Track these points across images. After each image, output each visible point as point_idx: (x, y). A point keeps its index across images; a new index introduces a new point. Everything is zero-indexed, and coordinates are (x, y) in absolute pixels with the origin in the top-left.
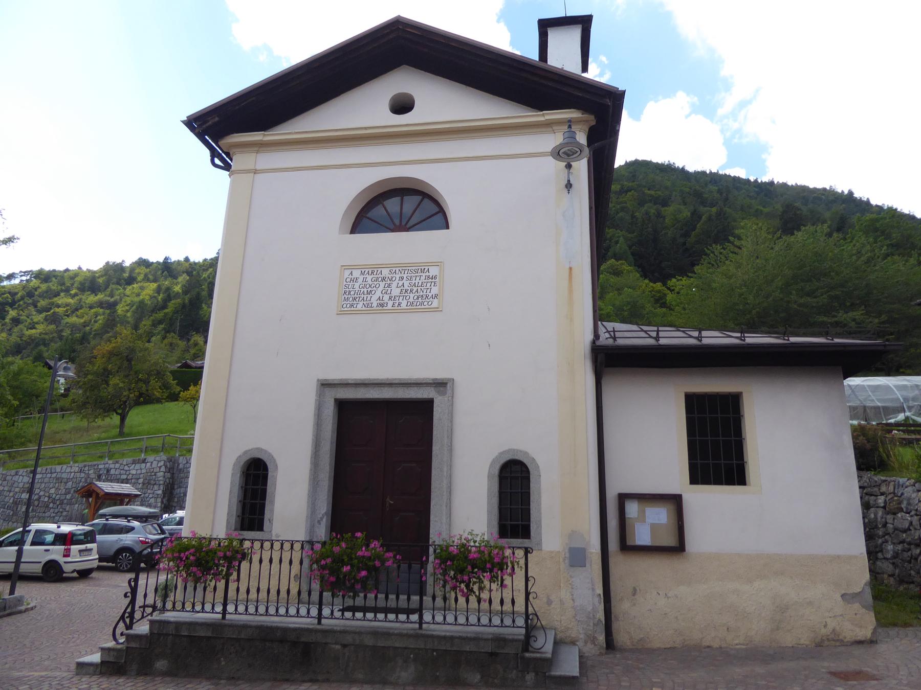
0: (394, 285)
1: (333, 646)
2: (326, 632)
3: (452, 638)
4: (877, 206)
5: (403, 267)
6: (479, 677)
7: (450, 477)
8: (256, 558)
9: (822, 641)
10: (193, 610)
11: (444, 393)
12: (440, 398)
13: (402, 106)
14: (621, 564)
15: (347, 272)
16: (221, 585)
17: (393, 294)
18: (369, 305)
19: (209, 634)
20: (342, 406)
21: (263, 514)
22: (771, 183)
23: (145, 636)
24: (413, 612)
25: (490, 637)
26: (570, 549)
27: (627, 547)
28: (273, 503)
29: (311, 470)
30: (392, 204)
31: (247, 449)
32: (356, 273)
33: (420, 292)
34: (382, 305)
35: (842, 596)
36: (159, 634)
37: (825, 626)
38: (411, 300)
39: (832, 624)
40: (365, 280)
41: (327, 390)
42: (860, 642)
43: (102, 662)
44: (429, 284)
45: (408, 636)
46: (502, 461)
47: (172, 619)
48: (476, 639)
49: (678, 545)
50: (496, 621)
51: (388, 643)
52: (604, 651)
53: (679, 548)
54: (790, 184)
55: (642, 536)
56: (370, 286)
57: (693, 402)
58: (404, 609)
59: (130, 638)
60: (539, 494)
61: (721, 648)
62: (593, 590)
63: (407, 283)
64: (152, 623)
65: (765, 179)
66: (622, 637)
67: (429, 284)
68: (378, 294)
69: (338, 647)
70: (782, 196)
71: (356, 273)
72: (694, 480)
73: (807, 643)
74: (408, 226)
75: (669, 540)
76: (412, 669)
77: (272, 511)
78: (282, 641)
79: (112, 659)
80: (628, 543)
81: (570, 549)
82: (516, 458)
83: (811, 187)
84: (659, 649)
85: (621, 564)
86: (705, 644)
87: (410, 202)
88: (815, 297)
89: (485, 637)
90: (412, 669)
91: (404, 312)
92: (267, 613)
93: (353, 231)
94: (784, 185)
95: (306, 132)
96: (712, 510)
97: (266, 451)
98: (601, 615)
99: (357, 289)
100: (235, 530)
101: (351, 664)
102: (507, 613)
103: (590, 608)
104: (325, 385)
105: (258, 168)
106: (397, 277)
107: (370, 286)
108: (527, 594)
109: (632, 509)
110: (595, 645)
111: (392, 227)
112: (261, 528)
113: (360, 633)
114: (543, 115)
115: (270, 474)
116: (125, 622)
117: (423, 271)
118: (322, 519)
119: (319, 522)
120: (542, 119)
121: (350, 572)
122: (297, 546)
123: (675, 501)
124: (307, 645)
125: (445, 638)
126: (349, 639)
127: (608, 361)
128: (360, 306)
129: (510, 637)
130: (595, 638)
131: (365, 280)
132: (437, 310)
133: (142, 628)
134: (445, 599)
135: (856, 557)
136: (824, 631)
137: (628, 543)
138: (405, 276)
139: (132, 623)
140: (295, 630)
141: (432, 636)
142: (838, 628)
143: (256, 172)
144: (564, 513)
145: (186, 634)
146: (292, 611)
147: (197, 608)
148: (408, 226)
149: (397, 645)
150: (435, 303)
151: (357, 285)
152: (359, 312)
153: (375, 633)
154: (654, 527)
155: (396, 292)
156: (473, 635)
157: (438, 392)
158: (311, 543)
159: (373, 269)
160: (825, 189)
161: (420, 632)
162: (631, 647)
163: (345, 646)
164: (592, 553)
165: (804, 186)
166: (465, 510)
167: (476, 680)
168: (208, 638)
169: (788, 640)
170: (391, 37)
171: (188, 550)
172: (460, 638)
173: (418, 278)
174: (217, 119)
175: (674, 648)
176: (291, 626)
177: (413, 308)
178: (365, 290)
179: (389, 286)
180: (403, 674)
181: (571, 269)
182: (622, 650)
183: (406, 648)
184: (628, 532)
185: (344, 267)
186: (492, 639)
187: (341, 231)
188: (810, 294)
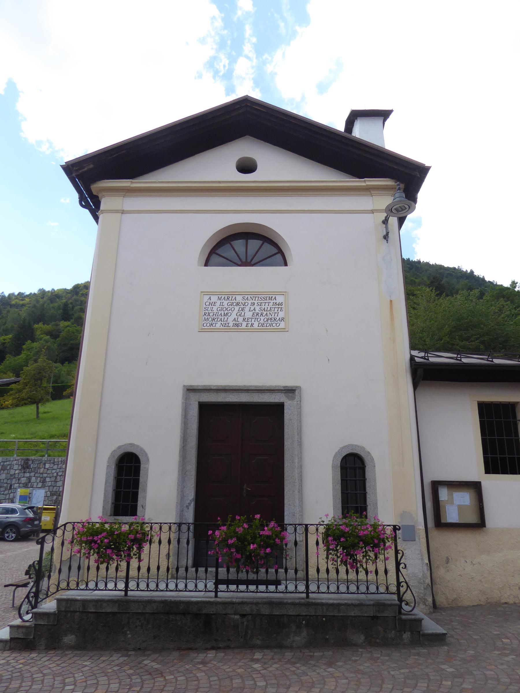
0: (247, 309)
1: (233, 616)
2: (225, 604)
3: (339, 605)
4: (489, 282)
5: (255, 295)
6: (363, 638)
7: (301, 467)
8: (156, 539)
10: (77, 588)
11: (293, 399)
12: (290, 402)
16: (124, 564)
17: (246, 317)
18: (226, 325)
19: (116, 610)
20: (203, 407)
21: (136, 500)
22: (419, 262)
23: (54, 614)
25: (372, 602)
28: (145, 491)
29: (180, 462)
30: (239, 244)
31: (121, 444)
32: (214, 299)
33: (269, 316)
34: (237, 325)
36: (65, 611)
38: (262, 322)
40: (222, 304)
41: (192, 395)
43: (11, 639)
44: (276, 309)
45: (300, 604)
46: (362, 454)
47: (79, 598)
48: (360, 605)
49: (480, 522)
50: (343, 588)
51: (284, 612)
52: (432, 610)
53: (480, 524)
54: (431, 263)
55: (452, 515)
56: (226, 309)
57: (486, 410)
58: (273, 581)
59: (36, 616)
61: (515, 603)
62: (422, 559)
63: (257, 308)
64: (59, 601)
65: (415, 259)
67: (276, 309)
68: (234, 316)
69: (237, 617)
70: (426, 271)
71: (214, 299)
72: (488, 471)
74: (253, 263)
75: (472, 519)
76: (305, 633)
77: (145, 498)
78: (184, 614)
79: (21, 636)
80: (443, 521)
82: (355, 452)
83: (446, 266)
84: (469, 606)
86: (503, 601)
87: (254, 244)
88: (472, 341)
89: (368, 603)
90: (305, 633)
91: (256, 331)
93: (206, 265)
94: (428, 264)
95: (169, 182)
97: (138, 446)
98: (428, 581)
99: (215, 311)
100: (110, 516)
101: (250, 632)
102: (352, 582)
103: (420, 575)
104: (190, 390)
105: (125, 209)
106: (250, 302)
107: (226, 309)
108: (398, 564)
109: (443, 493)
110: (426, 605)
111: (240, 263)
112: (134, 513)
113: (257, 604)
114: (365, 181)
115: (142, 466)
116: (30, 602)
117: (271, 299)
118: (190, 504)
119: (187, 507)
121: (255, 549)
122: (165, 528)
123: (476, 487)
124: (207, 615)
125: (332, 605)
126: (247, 609)
127: (423, 375)
128: (218, 325)
129: (389, 602)
130: (425, 599)
131: (222, 304)
132: (284, 330)
133: (49, 605)
134: (337, 572)
137: (443, 521)
138: (256, 302)
139: (36, 602)
140: (197, 603)
141: (322, 604)
143: (123, 212)
145: (93, 611)
146: (162, 586)
147: (103, 585)
148: (253, 263)
149: (291, 613)
150: (282, 325)
151: (215, 308)
152: (218, 331)
153: (271, 603)
154: (460, 507)
155: (249, 315)
156: (357, 602)
157: (288, 398)
158: (180, 525)
159: (229, 296)
160: (454, 268)
161: (218, 600)
162: (447, 606)
163: (243, 616)
164: (419, 529)
165: (441, 266)
166: (313, 497)
167: (361, 641)
168: (114, 614)
170: (241, 111)
171: (101, 533)
172: (346, 605)
173: (267, 304)
174: (92, 166)
175: (480, 605)
176: (192, 599)
177: (263, 328)
178: (223, 312)
179: (243, 309)
180: (297, 639)
181: (391, 301)
182: (443, 609)
183: (298, 615)
186: (373, 605)
188: (468, 339)
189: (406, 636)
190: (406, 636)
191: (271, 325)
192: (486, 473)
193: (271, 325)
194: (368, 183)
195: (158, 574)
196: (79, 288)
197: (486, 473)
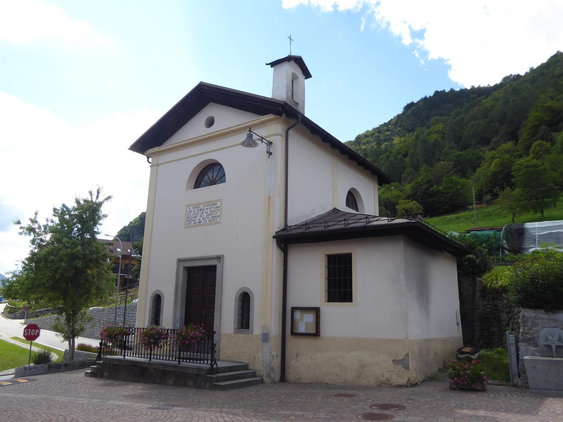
0: (204, 213)
5: (207, 203)
6: (192, 383)
9: (381, 384)
10: (144, 357)
13: (210, 122)
14: (291, 342)
15: (188, 208)
24: (204, 360)
26: (263, 334)
27: (294, 334)
32: (191, 208)
35: (393, 361)
37: (383, 376)
39: (387, 375)
42: (401, 386)
53: (317, 334)
55: (301, 328)
60: (253, 307)
62: (271, 353)
63: (209, 211)
66: (291, 375)
73: (374, 384)
75: (313, 330)
76: (173, 379)
80: (296, 331)
81: (263, 334)
85: (292, 343)
90: (173, 379)
92: (144, 357)
93: (194, 188)
96: (335, 315)
104: (180, 261)
105: (159, 163)
109: (298, 315)
120: (259, 121)
123: (316, 311)
132: (219, 223)
135: (401, 340)
136: (382, 379)
142: (389, 377)
144: (265, 316)
158: (174, 330)
159: (196, 206)
163: (154, 369)
169: (364, 382)
184: (297, 325)
185: (187, 206)
187: (188, 188)
189: (208, 384)
190: (208, 384)
191: (214, 220)
192: (351, 301)
193: (214, 220)
194: (261, 120)
195: (163, 355)
196: (360, 138)
197: (351, 301)
